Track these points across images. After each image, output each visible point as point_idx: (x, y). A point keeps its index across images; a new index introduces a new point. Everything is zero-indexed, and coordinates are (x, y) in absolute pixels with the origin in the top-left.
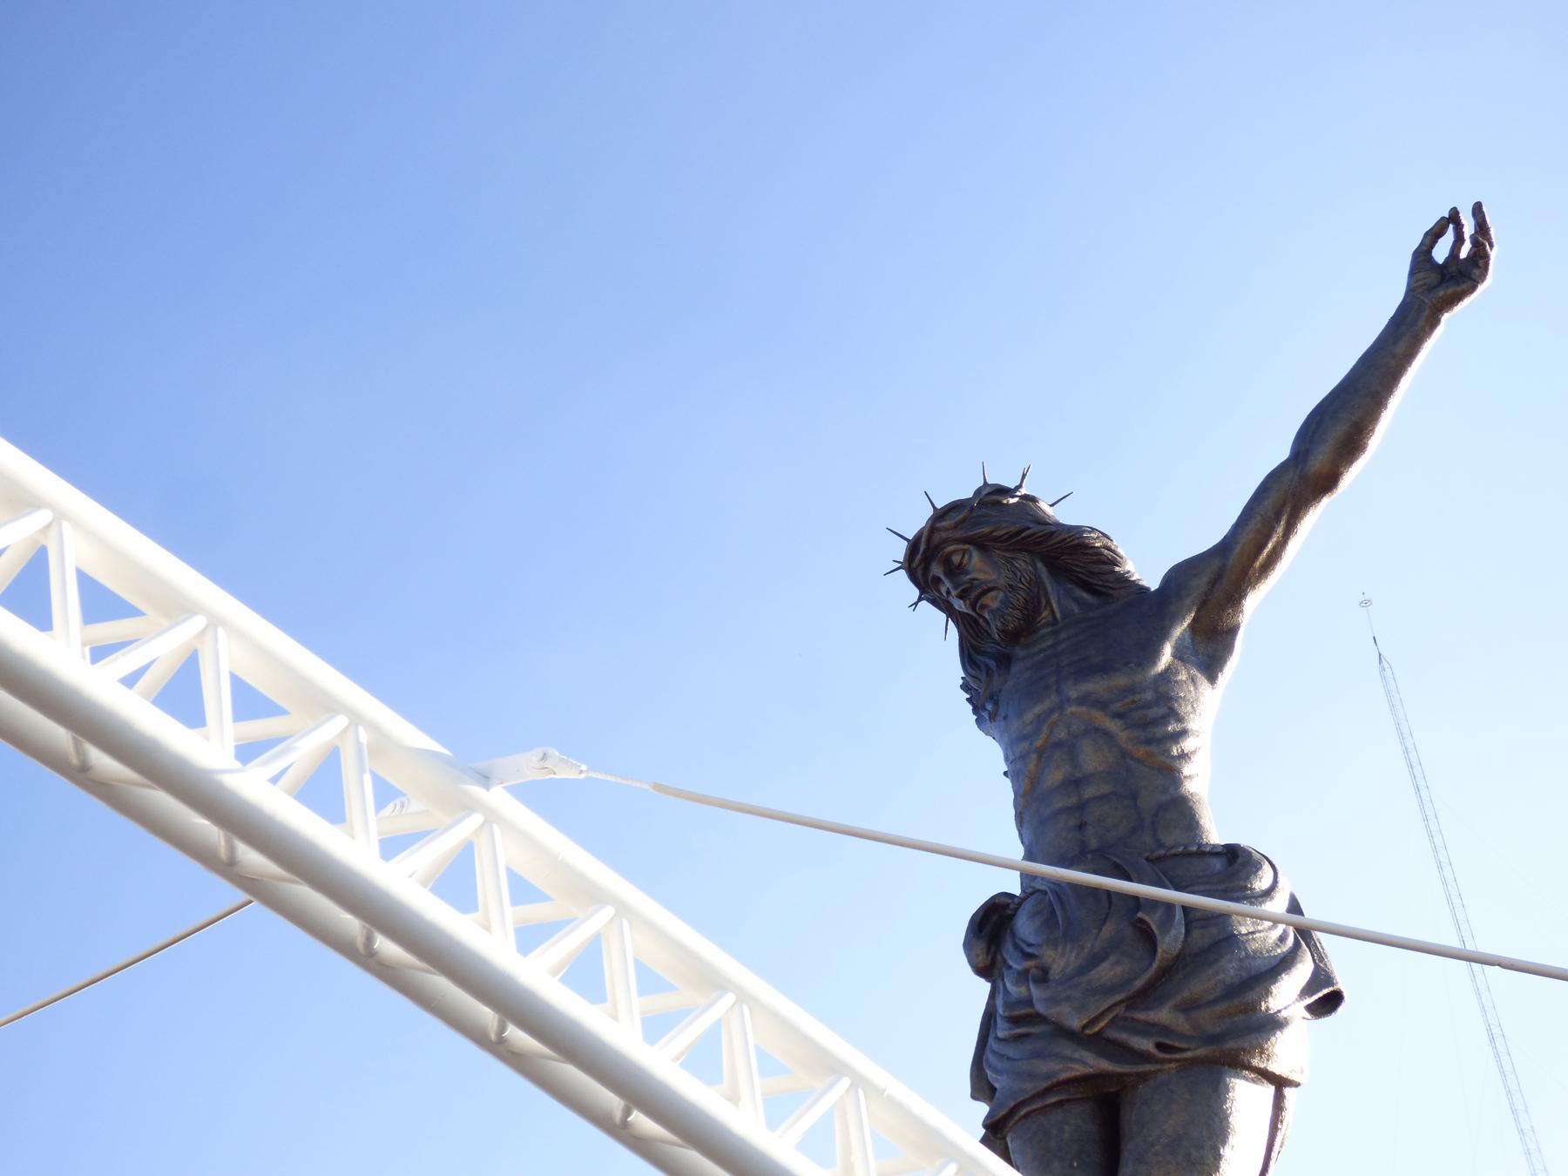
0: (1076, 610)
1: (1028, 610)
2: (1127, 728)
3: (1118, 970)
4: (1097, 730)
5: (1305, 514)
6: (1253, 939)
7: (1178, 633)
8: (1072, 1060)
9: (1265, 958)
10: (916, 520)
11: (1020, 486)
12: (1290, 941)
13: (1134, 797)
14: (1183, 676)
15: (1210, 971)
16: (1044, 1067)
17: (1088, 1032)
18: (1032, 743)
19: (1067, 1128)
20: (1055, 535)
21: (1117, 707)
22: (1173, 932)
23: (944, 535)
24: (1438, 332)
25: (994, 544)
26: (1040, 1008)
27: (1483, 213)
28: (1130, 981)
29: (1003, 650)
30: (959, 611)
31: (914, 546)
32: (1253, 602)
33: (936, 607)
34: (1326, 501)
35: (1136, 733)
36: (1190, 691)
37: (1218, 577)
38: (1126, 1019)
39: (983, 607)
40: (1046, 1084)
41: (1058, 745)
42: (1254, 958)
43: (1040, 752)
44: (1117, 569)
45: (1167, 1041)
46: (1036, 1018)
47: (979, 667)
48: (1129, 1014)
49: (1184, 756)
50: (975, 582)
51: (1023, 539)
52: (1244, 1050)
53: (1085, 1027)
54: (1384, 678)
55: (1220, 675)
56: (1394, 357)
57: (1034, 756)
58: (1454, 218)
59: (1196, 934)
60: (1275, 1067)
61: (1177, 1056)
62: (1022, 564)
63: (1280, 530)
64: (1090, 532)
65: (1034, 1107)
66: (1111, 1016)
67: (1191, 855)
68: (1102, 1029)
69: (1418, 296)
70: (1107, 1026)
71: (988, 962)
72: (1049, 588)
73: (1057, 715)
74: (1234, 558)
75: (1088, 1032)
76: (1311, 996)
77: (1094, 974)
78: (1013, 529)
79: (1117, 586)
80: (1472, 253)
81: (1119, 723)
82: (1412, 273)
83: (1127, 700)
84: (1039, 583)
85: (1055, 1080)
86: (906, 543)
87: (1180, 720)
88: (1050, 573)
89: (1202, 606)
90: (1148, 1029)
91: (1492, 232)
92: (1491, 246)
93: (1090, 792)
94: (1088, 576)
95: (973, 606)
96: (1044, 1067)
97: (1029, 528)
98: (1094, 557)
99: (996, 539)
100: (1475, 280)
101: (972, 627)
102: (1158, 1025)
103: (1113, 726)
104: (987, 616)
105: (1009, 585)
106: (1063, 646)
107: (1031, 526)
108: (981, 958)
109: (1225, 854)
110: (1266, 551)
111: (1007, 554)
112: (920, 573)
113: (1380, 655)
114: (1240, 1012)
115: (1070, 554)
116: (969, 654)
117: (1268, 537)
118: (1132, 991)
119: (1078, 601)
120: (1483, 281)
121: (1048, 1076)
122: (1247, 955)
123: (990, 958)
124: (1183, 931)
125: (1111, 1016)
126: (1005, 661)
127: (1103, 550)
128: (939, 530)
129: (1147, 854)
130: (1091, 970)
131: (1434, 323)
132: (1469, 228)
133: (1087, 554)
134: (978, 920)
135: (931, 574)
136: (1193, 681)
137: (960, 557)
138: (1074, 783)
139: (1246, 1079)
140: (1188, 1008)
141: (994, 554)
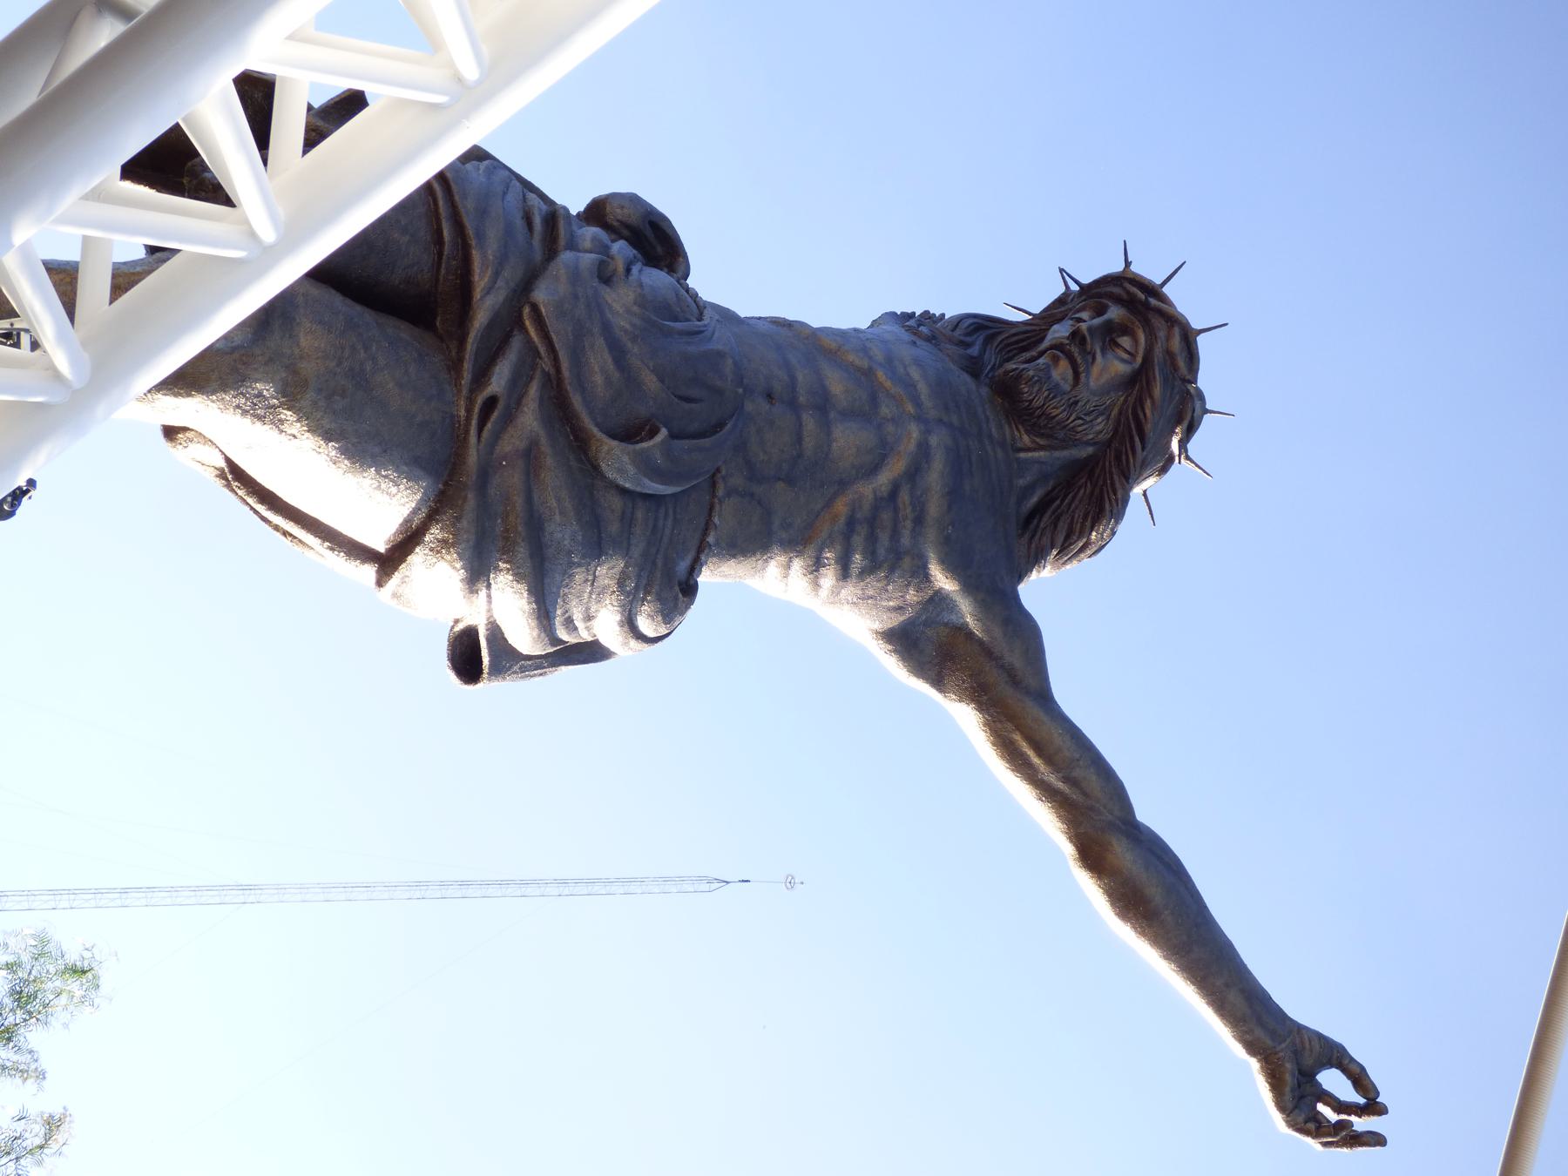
0: (1021, 482)
1: (1039, 417)
2: (876, 499)
3: (599, 379)
4: (883, 457)
5: (1060, 817)
6: (587, 580)
7: (963, 607)
8: (497, 274)
9: (559, 588)
10: (1185, 299)
12: (563, 634)
13: (790, 481)
14: (912, 596)
15: (568, 505)
16: (493, 235)
17: (526, 310)
19: (406, 238)
20: (1124, 481)
21: (904, 496)
22: (631, 470)
23: (1162, 334)
24: (1238, 1050)
25: (1134, 396)
26: (566, 257)
27: (1375, 1146)
28: (582, 388)
30: (1048, 329)
31: (1152, 291)
32: (966, 718)
33: (1054, 303)
34: (1068, 849)
35: (866, 506)
36: (889, 600)
37: (1014, 680)
38: (533, 367)
39: (1056, 360)
40: (470, 232)
41: (874, 400)
42: (565, 573)
43: (868, 373)
44: (1055, 552)
45: (496, 414)
46: (551, 251)
47: (969, 334)
48: (538, 375)
49: (816, 566)
52: (458, 519)
53: (535, 308)
54: (700, 879)
55: (890, 647)
56: (1227, 985)
57: (865, 364)
58: (1373, 1107)
59: (616, 502)
60: (418, 559)
61: (474, 422)
62: (1098, 428)
63: (1052, 779)
65: (441, 203)
66: (542, 350)
67: (705, 532)
68: (527, 332)
69: (1291, 1037)
70: (529, 341)
71: (610, 219)
72: (1057, 454)
74: (1033, 710)
75: (526, 310)
76: (488, 640)
77: (600, 342)
78: (1148, 427)
79: (1033, 546)
80: (1320, 1117)
82: (1320, 1036)
83: (909, 510)
85: (473, 243)
87: (863, 574)
89: (987, 651)
90: (518, 384)
91: (1345, 1150)
92: (1325, 1144)
93: (810, 423)
94: (1053, 513)
95: (1058, 346)
96: (493, 235)
97: (1143, 448)
99: (1140, 402)
100: (1291, 1112)
101: (1017, 342)
102: (517, 409)
103: (884, 479)
104: (1041, 361)
105: (1078, 401)
106: (989, 448)
107: (1145, 453)
108: (618, 211)
109: (688, 579)
110: (1031, 753)
111: (1115, 412)
112: (1116, 290)
113: (727, 882)
114: (507, 531)
115: (1092, 493)
116: (987, 328)
117: (1049, 760)
118: (569, 388)
119: (1030, 489)
120: (1287, 1122)
121: (480, 236)
122: (571, 565)
123: (615, 224)
124: (627, 485)
125: (542, 350)
126: (973, 368)
127: (1085, 540)
128: (1171, 328)
129: (724, 472)
130: (606, 339)
131: (1252, 1048)
132: (1360, 1124)
133: (1085, 518)
134: (662, 224)
136: (899, 609)
137: (1128, 348)
138: (823, 404)
139: (414, 512)
140: (530, 455)
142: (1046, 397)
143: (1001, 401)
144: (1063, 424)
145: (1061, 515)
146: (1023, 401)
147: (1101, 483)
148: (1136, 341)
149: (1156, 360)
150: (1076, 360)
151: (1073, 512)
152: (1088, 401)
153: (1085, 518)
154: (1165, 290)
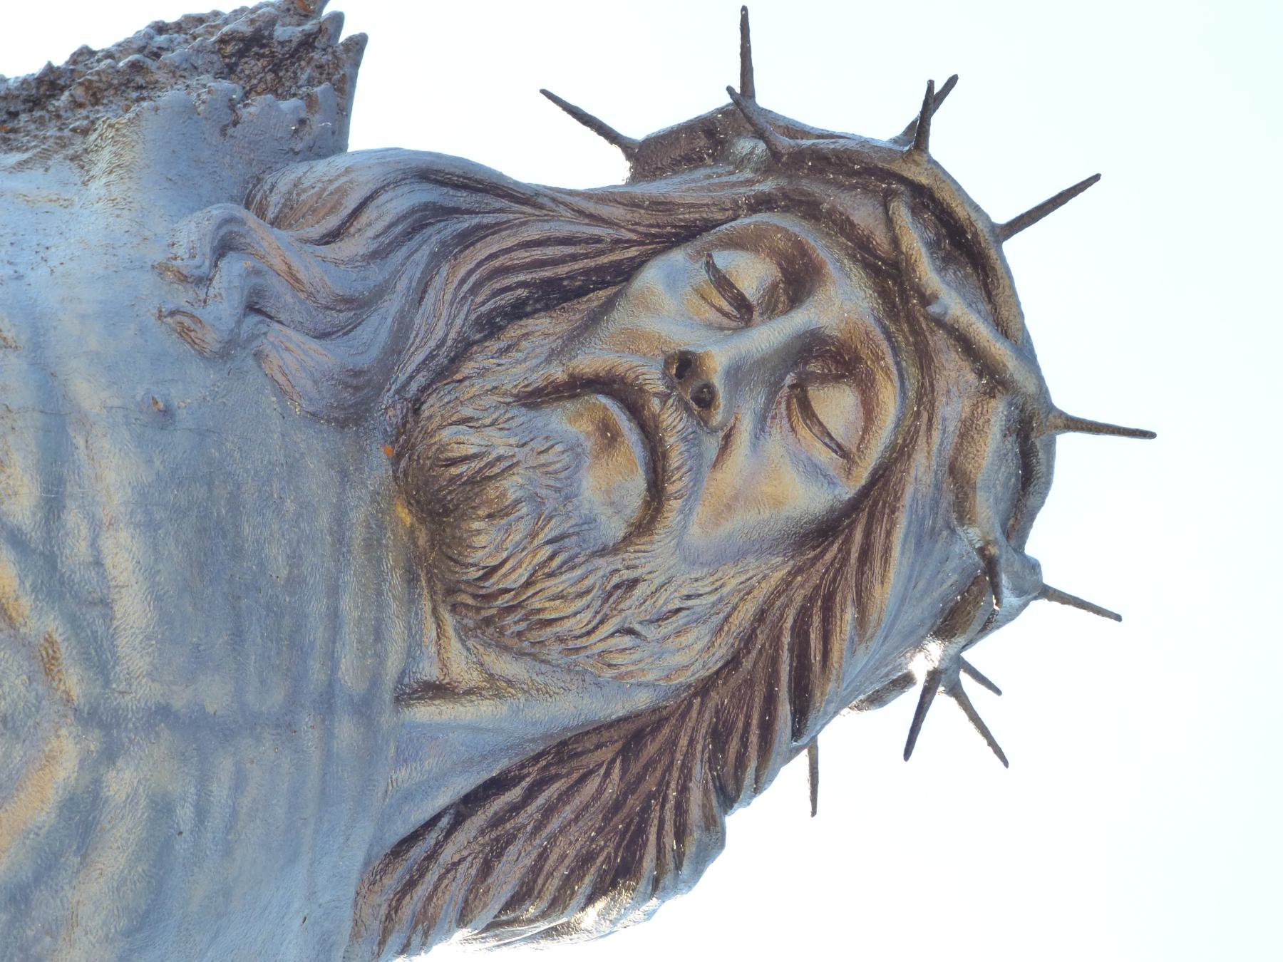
23: (951, 410)
50: (711, 445)
51: (770, 701)
73: (76, 692)
86: (1001, 216)
94: (497, 821)
98: (555, 882)
105: (635, 582)
111: (747, 611)
112: (864, 214)
115: (617, 806)
142: (543, 565)
143: (408, 520)
144: (571, 645)
145: (511, 838)
146: (467, 566)
147: (650, 784)
148: (869, 410)
149: (909, 490)
150: (665, 456)
151: (553, 839)
152: (669, 581)
153: (585, 860)
154: (1013, 249)
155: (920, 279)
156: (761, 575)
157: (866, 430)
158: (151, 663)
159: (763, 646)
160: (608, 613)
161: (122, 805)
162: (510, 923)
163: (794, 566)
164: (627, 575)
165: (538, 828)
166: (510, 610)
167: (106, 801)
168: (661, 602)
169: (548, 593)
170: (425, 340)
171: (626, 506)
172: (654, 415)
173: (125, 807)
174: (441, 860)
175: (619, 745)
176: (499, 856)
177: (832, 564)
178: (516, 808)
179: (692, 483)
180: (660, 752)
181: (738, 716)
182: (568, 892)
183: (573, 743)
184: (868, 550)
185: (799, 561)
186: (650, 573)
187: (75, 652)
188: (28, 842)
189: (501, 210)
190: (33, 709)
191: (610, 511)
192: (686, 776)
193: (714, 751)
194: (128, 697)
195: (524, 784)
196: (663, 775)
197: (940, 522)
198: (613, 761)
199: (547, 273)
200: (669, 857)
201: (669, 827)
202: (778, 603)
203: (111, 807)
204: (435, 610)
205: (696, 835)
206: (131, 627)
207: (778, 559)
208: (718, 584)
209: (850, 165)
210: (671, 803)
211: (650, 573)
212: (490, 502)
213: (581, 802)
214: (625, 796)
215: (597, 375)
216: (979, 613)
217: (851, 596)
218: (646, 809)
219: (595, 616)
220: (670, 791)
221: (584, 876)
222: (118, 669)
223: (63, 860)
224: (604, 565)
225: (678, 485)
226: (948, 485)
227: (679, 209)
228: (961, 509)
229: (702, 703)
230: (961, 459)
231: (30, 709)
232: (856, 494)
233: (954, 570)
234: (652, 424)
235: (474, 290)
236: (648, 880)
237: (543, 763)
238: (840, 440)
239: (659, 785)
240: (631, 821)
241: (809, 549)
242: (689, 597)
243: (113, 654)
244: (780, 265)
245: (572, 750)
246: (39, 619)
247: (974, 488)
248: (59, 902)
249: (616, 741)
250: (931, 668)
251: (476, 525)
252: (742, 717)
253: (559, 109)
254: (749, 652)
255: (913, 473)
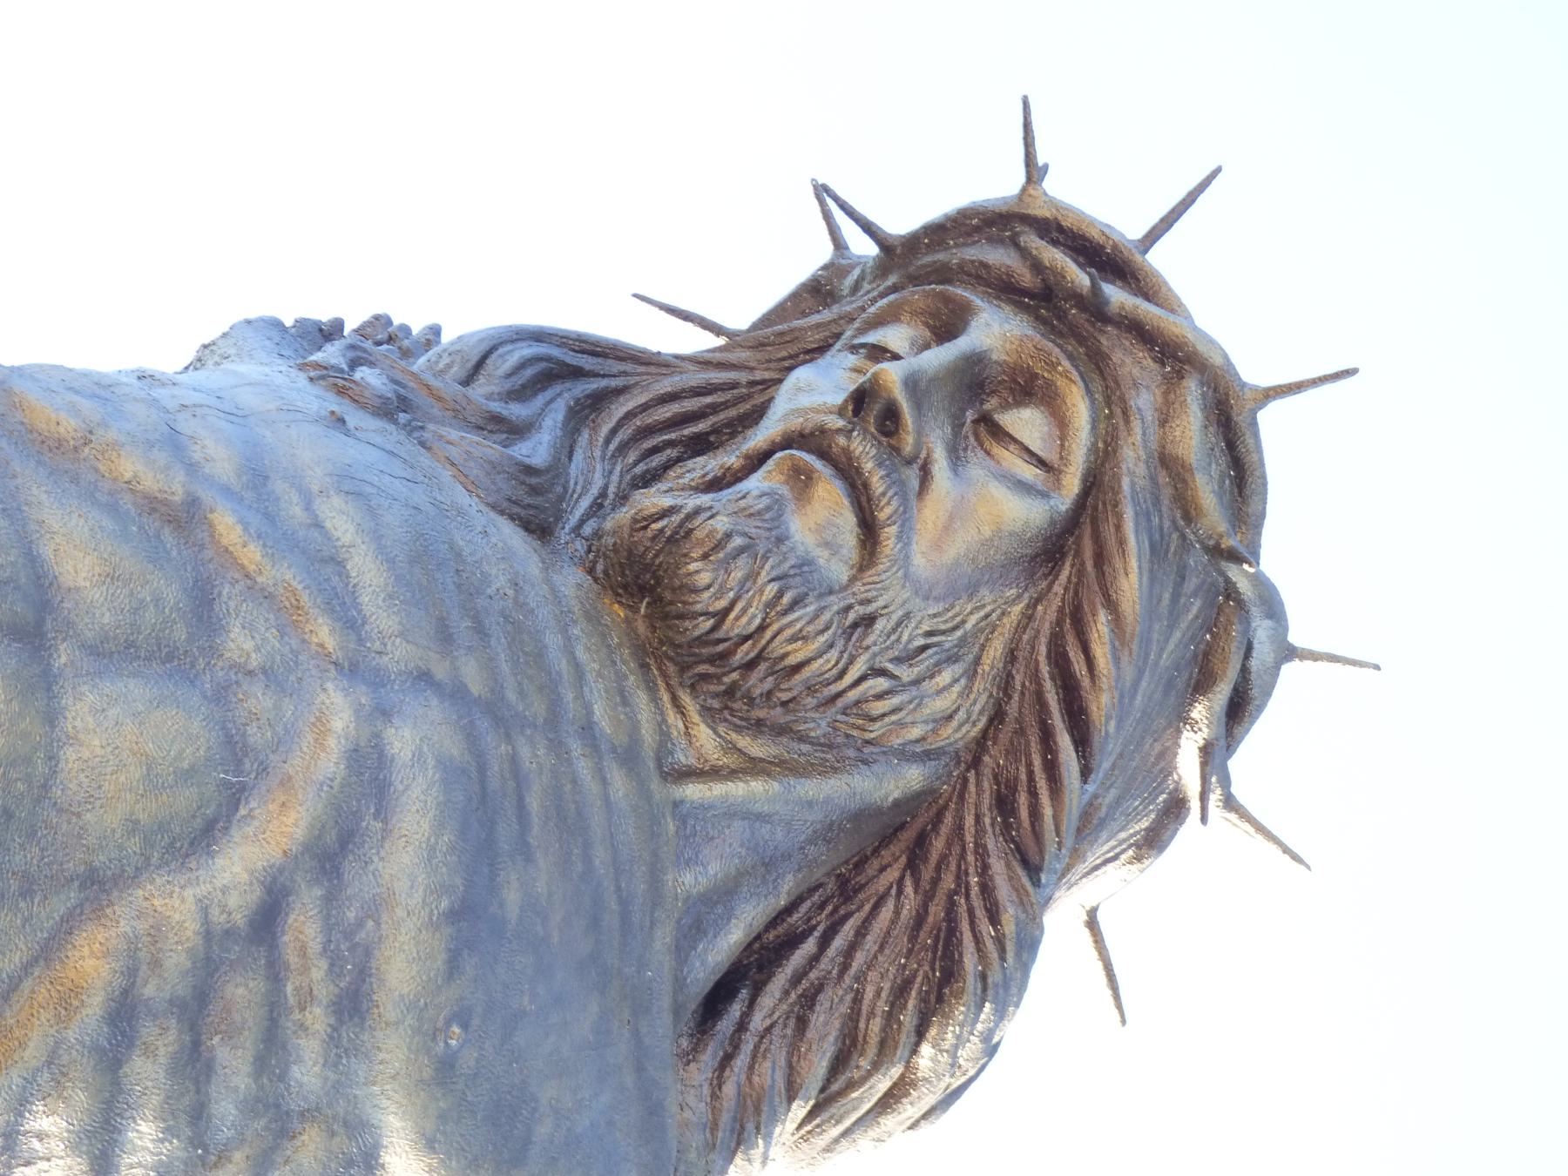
0: (689, 881)
1: (750, 665)
2: (208, 935)
4: (235, 796)
11: (1230, 803)
18: (226, 491)
23: (1144, 401)
29: (574, 519)
35: (177, 960)
39: (801, 479)
47: (520, 394)
50: (912, 476)
51: (1047, 736)
57: (176, 487)
62: (942, 704)
64: (987, 1037)
72: (813, 788)
73: (331, 644)
81: (239, 905)
84: (866, 754)
88: (861, 816)
94: (796, 979)
97: (1086, 773)
98: (876, 1025)
99: (1076, 618)
104: (755, 483)
106: (584, 768)
111: (996, 651)
112: (998, 257)
115: (920, 919)
116: (577, 373)
119: (722, 897)
127: (896, 1071)
135: (978, 302)
141: (1011, 592)
142: (771, 604)
145: (819, 988)
147: (948, 882)
150: (866, 485)
153: (901, 992)
155: (1072, 283)
156: (999, 611)
157: (1063, 438)
158: (400, 623)
159: (1023, 685)
160: (854, 653)
161: (410, 764)
162: (842, 1093)
163: (1031, 598)
164: (860, 610)
165: (845, 967)
166: (750, 665)
167: (392, 761)
168: (905, 638)
169: (788, 633)
170: (585, 491)
171: (841, 546)
172: (843, 449)
173: (413, 765)
174: (751, 1027)
175: (903, 859)
176: (811, 1007)
177: (1069, 581)
178: (815, 959)
179: (901, 509)
180: (949, 844)
181: (1018, 769)
182: (895, 1026)
183: (855, 877)
184: (1102, 553)
185: (1033, 592)
186: (885, 607)
187: (319, 600)
188: (323, 794)
189: (625, 374)
190: (291, 663)
191: (826, 553)
192: (982, 856)
193: (1005, 821)
194: (386, 658)
195: (816, 934)
196: (959, 866)
197: (1167, 524)
198: (902, 879)
199: (689, 430)
200: (990, 945)
201: (980, 913)
202: (1025, 637)
203: (399, 765)
204: (675, 699)
205: (1011, 911)
206: (370, 586)
207: (1012, 592)
208: (958, 619)
209: (968, 222)
210: (975, 891)
211: (885, 607)
212: (700, 543)
213: (881, 929)
214: (925, 906)
215: (773, 442)
216: (1234, 646)
217: (1099, 599)
218: (951, 907)
219: (842, 657)
220: (970, 878)
221: (906, 1002)
222: (367, 627)
223: (364, 824)
224: (836, 603)
225: (888, 511)
226: (1163, 478)
227: (806, 333)
228: (1183, 502)
229: (977, 774)
230: (1169, 446)
231: (288, 664)
232: (1072, 504)
233: (1195, 594)
234: (844, 459)
235: (623, 448)
236: (975, 977)
237: (830, 908)
238: (1039, 453)
239: (958, 877)
240: (939, 930)
241: (1040, 579)
242: (930, 634)
243: (360, 612)
244: (927, 325)
245: (856, 883)
246: (273, 566)
247: (1191, 470)
248: (371, 877)
249: (900, 856)
250: (1202, 743)
251: (693, 567)
252: (1023, 769)
253: (656, 309)
254: (1010, 698)
255: (1124, 467)
